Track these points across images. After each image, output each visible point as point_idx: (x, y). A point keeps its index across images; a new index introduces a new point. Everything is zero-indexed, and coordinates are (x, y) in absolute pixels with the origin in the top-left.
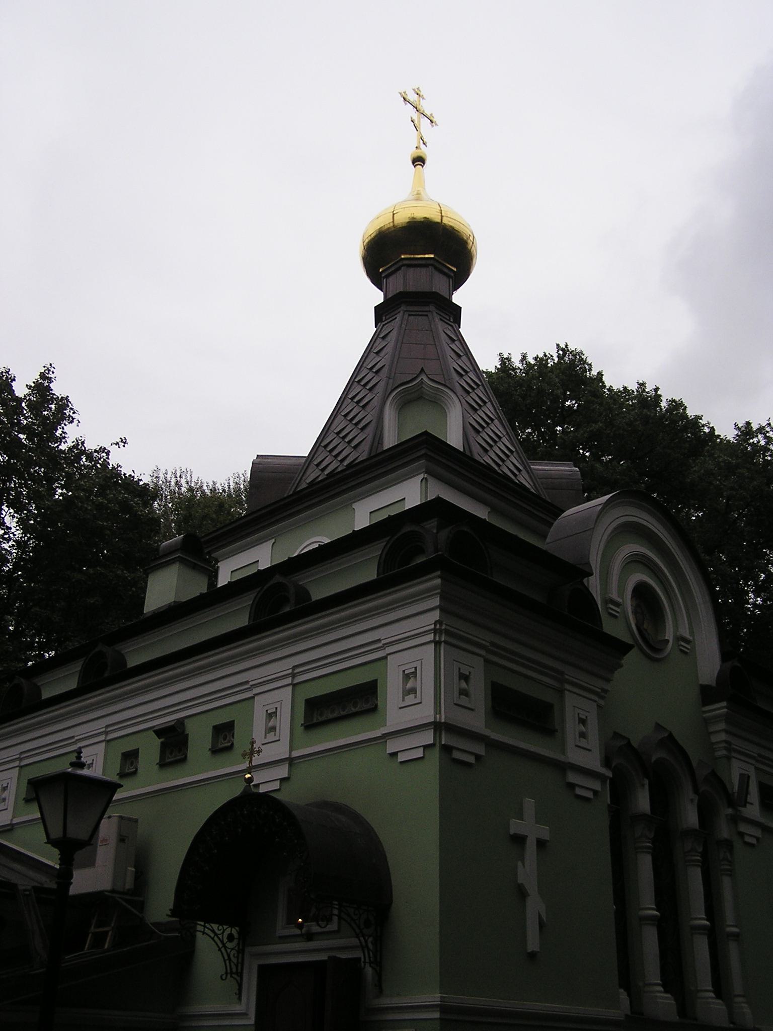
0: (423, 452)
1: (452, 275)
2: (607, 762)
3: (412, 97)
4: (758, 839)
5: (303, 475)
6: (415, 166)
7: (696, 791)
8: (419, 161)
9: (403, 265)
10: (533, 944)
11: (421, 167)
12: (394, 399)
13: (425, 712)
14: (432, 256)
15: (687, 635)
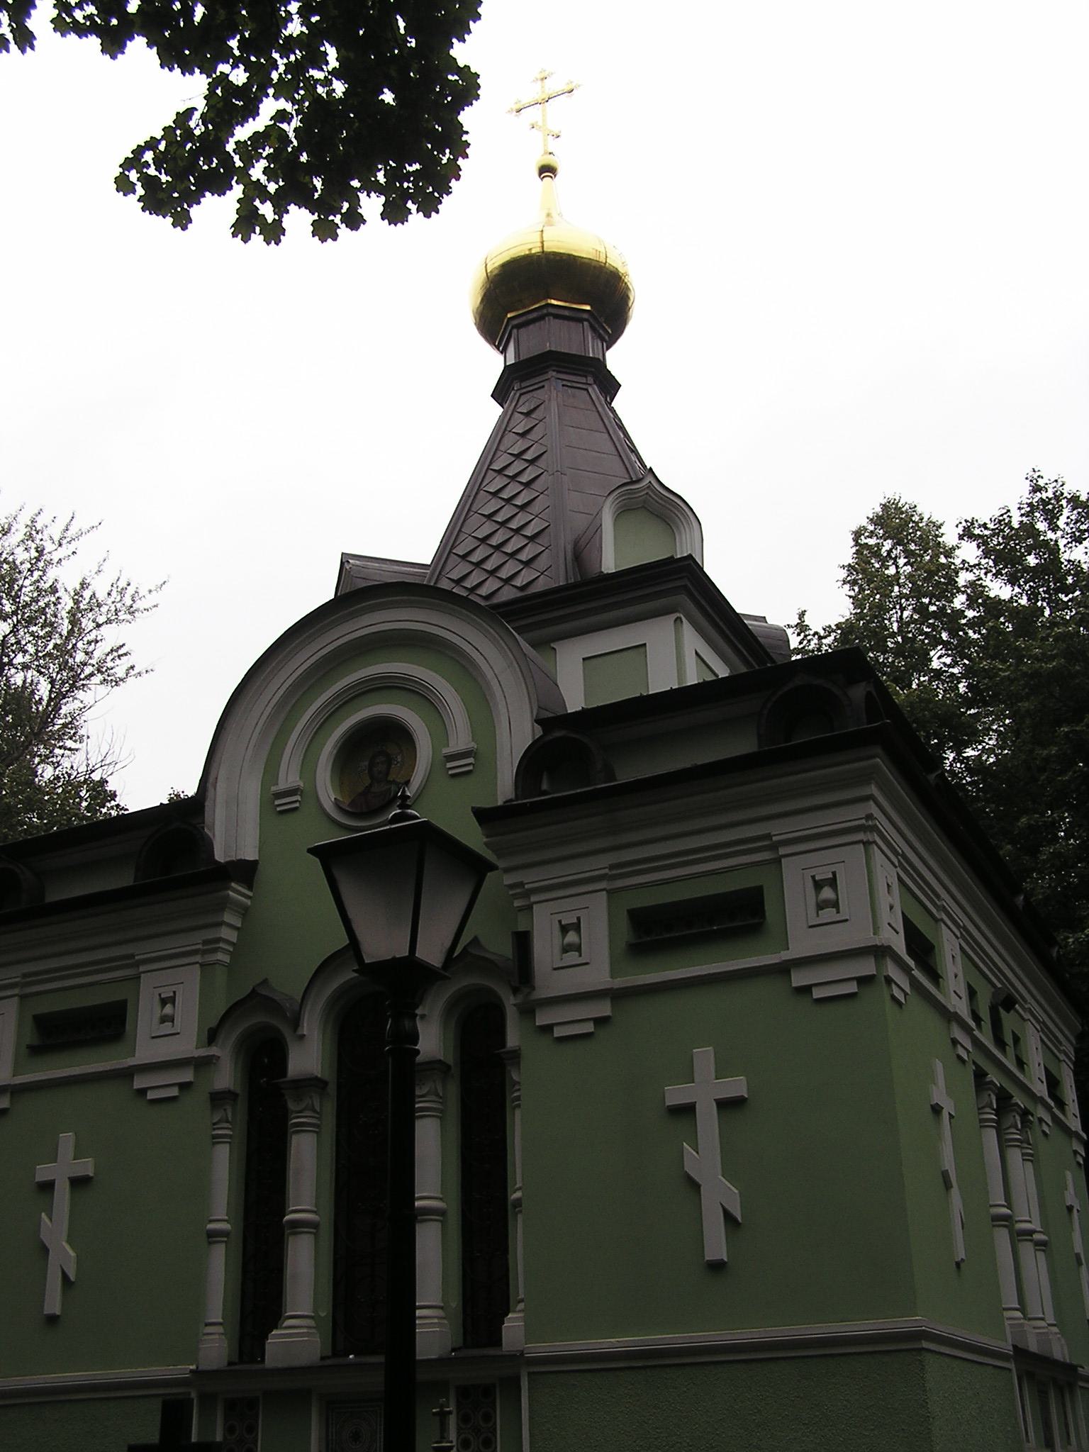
1: (607, 338)
6: (542, 179)
8: (547, 170)
9: (549, 314)
10: (716, 1246)
11: (549, 178)
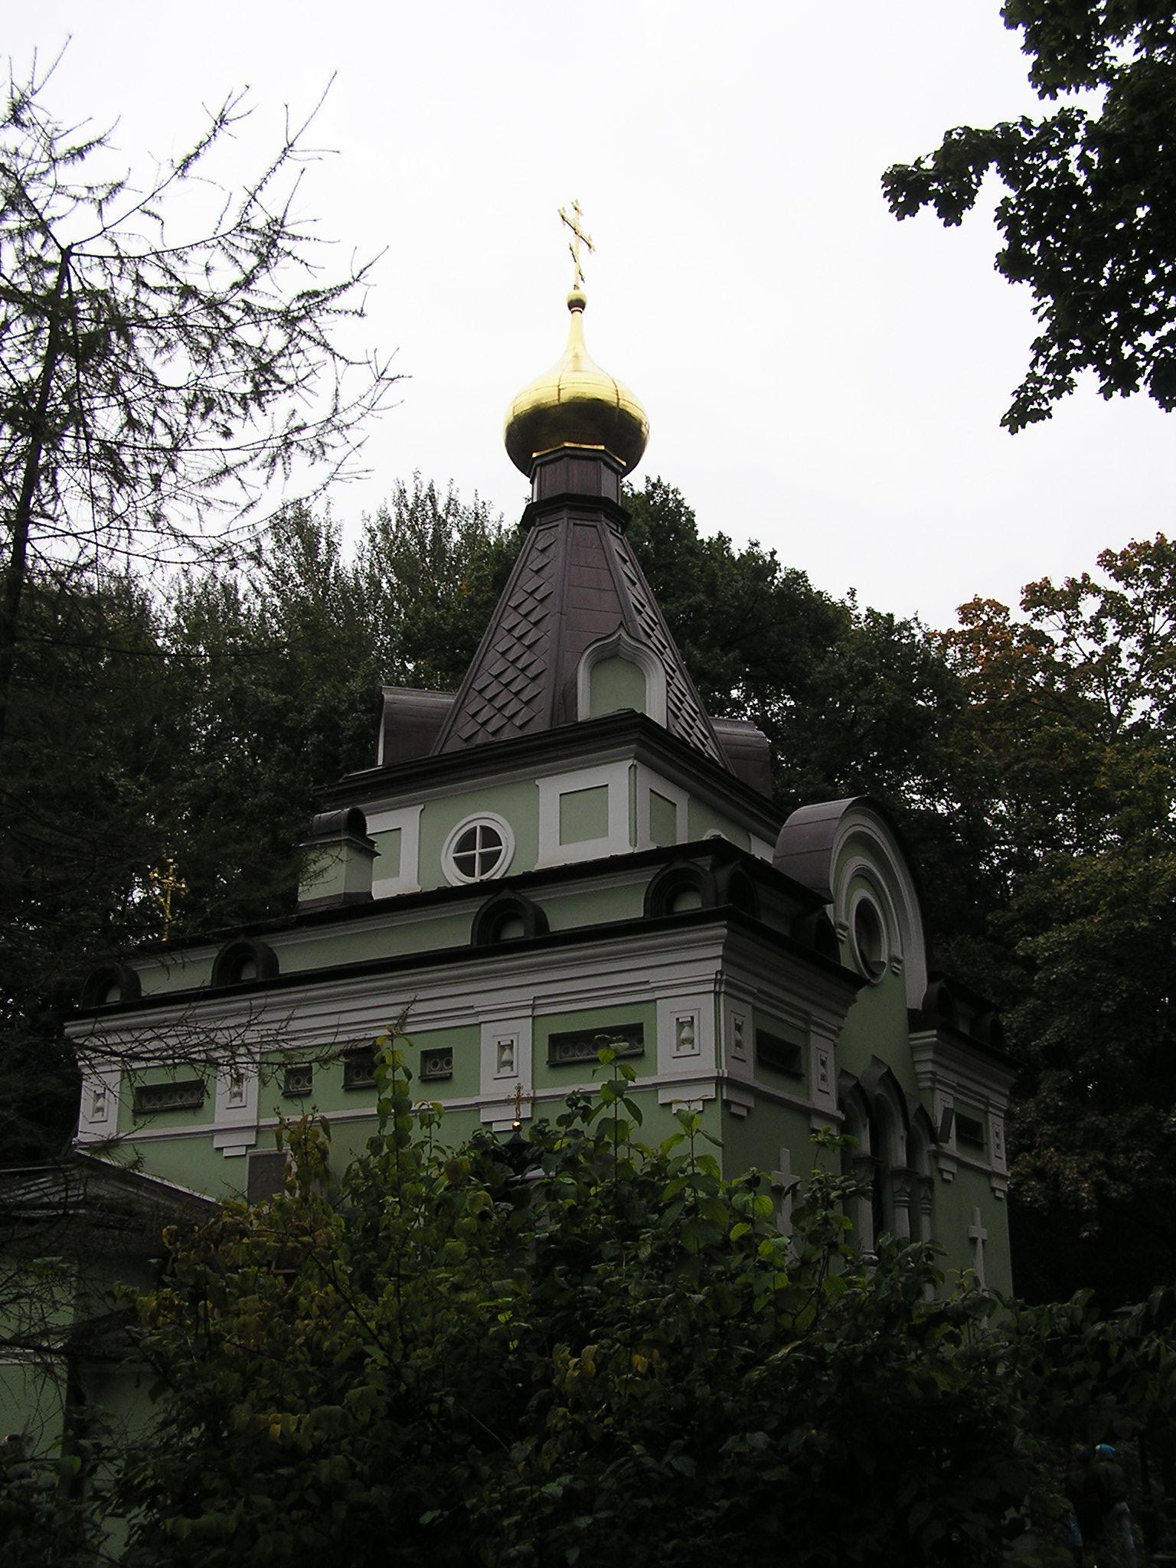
0: (636, 736)
2: (841, 1105)
3: (571, 215)
4: (749, 1109)
5: (452, 726)
7: (907, 1127)
9: (567, 455)
12: (589, 656)
13: (705, 1065)
14: (602, 448)
15: (900, 956)
